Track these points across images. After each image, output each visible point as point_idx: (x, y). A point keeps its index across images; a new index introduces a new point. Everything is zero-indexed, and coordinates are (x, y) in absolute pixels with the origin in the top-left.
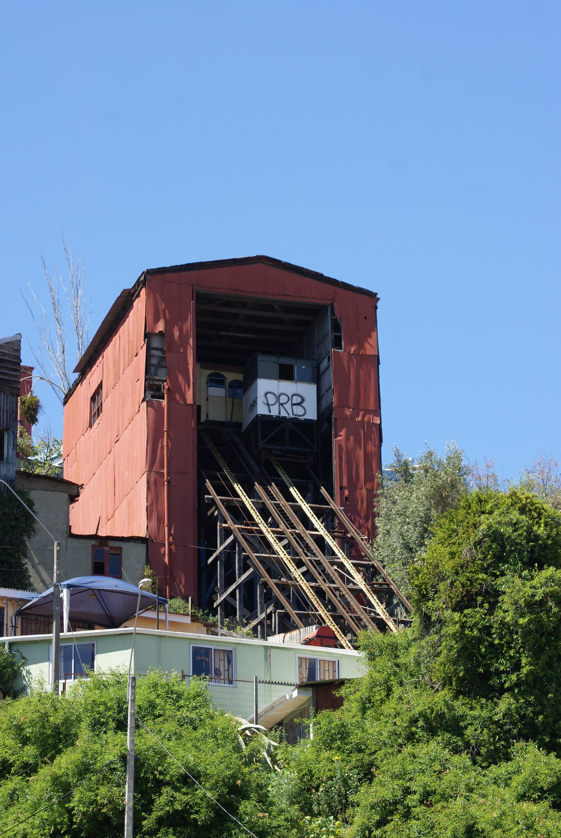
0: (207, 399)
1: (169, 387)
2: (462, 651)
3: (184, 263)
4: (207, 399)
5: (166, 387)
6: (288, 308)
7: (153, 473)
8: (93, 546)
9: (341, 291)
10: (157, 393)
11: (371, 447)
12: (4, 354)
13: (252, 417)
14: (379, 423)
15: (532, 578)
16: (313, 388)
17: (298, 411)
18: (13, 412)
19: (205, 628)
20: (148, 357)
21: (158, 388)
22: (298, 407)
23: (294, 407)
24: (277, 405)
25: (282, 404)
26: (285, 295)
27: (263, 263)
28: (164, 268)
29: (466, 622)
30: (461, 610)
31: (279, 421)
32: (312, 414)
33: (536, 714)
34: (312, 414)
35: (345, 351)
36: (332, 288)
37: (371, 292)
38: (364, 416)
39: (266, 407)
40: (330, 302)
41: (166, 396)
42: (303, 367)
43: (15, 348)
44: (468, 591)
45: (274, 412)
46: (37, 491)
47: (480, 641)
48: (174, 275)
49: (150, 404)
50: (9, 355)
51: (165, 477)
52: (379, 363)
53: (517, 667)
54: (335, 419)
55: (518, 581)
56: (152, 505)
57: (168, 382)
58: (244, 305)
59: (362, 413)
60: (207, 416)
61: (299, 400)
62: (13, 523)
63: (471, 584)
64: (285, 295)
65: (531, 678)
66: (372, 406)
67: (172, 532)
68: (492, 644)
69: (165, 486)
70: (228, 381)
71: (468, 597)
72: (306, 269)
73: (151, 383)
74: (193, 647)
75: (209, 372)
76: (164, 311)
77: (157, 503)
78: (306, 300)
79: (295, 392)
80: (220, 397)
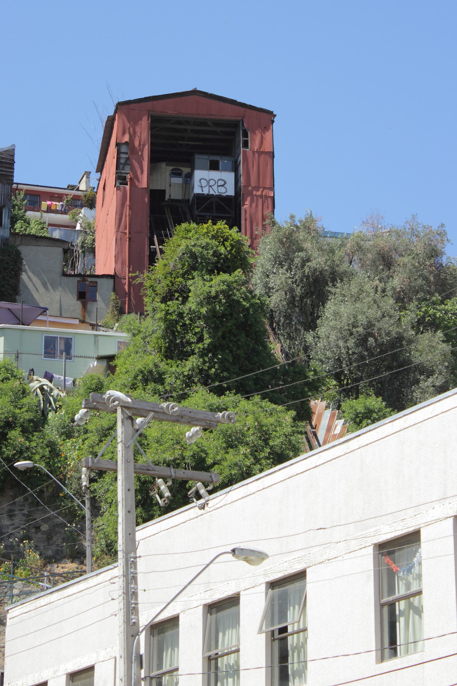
0: (170, 186)
1: (131, 177)
2: (167, 328)
3: (143, 97)
4: (170, 186)
5: (129, 177)
6: (218, 123)
7: (119, 233)
8: (78, 281)
9: (249, 111)
10: (124, 182)
11: (267, 212)
12: (3, 158)
13: (192, 196)
14: (273, 196)
15: (211, 280)
16: (232, 175)
17: (222, 190)
18: (8, 195)
19: (91, 327)
20: (118, 159)
21: (125, 178)
22: (222, 187)
23: (219, 187)
24: (208, 187)
25: (211, 186)
26: (211, 115)
27: (197, 95)
28: (130, 100)
29: (168, 310)
30: (166, 302)
31: (208, 197)
32: (231, 192)
33: (210, 368)
34: (231, 192)
35: (251, 150)
36: (242, 109)
37: (269, 111)
38: (262, 191)
39: (200, 188)
40: (241, 118)
41: (129, 183)
42: (226, 162)
43: (11, 154)
44: (170, 290)
45: (206, 192)
46: (42, 247)
47: (177, 322)
48: (136, 105)
49: (118, 188)
50: (6, 159)
51: (127, 236)
52: (273, 157)
53: (201, 339)
54: (243, 194)
55: (201, 283)
56: (118, 253)
57: (131, 174)
58: (188, 123)
59: (261, 189)
60: (170, 196)
61: (222, 183)
62: (5, 266)
63: (173, 285)
64: (211, 115)
65: (211, 347)
66: (268, 185)
67: (131, 270)
68: (184, 325)
69: (127, 242)
70: (184, 174)
71: (170, 293)
72: (225, 98)
73: (120, 175)
74: (45, 336)
75: (171, 168)
76: (129, 129)
77: (122, 252)
78: (224, 118)
79: (220, 178)
80: (179, 184)
